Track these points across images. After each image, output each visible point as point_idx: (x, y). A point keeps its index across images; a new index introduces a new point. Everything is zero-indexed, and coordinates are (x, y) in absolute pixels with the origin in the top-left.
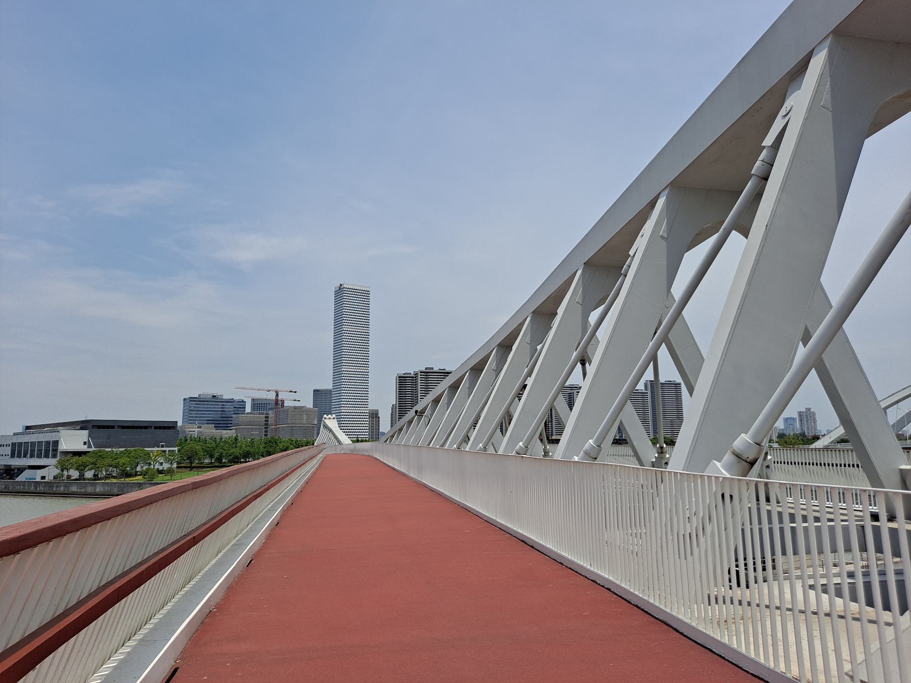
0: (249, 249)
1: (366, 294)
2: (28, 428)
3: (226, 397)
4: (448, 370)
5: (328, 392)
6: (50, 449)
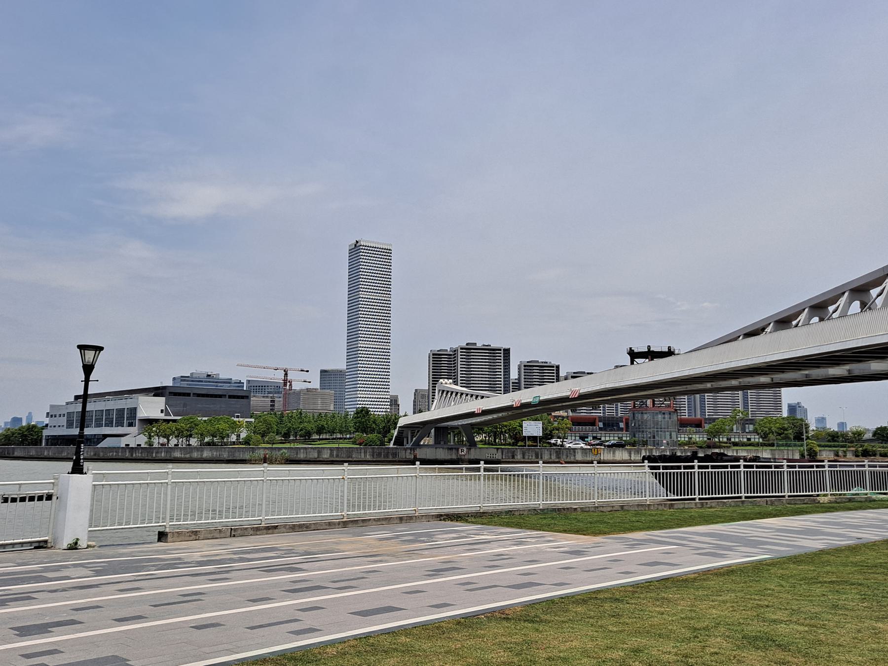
0: (198, 198)
1: (387, 252)
3: (223, 376)
4: (493, 346)
5: (339, 374)
6: (129, 417)
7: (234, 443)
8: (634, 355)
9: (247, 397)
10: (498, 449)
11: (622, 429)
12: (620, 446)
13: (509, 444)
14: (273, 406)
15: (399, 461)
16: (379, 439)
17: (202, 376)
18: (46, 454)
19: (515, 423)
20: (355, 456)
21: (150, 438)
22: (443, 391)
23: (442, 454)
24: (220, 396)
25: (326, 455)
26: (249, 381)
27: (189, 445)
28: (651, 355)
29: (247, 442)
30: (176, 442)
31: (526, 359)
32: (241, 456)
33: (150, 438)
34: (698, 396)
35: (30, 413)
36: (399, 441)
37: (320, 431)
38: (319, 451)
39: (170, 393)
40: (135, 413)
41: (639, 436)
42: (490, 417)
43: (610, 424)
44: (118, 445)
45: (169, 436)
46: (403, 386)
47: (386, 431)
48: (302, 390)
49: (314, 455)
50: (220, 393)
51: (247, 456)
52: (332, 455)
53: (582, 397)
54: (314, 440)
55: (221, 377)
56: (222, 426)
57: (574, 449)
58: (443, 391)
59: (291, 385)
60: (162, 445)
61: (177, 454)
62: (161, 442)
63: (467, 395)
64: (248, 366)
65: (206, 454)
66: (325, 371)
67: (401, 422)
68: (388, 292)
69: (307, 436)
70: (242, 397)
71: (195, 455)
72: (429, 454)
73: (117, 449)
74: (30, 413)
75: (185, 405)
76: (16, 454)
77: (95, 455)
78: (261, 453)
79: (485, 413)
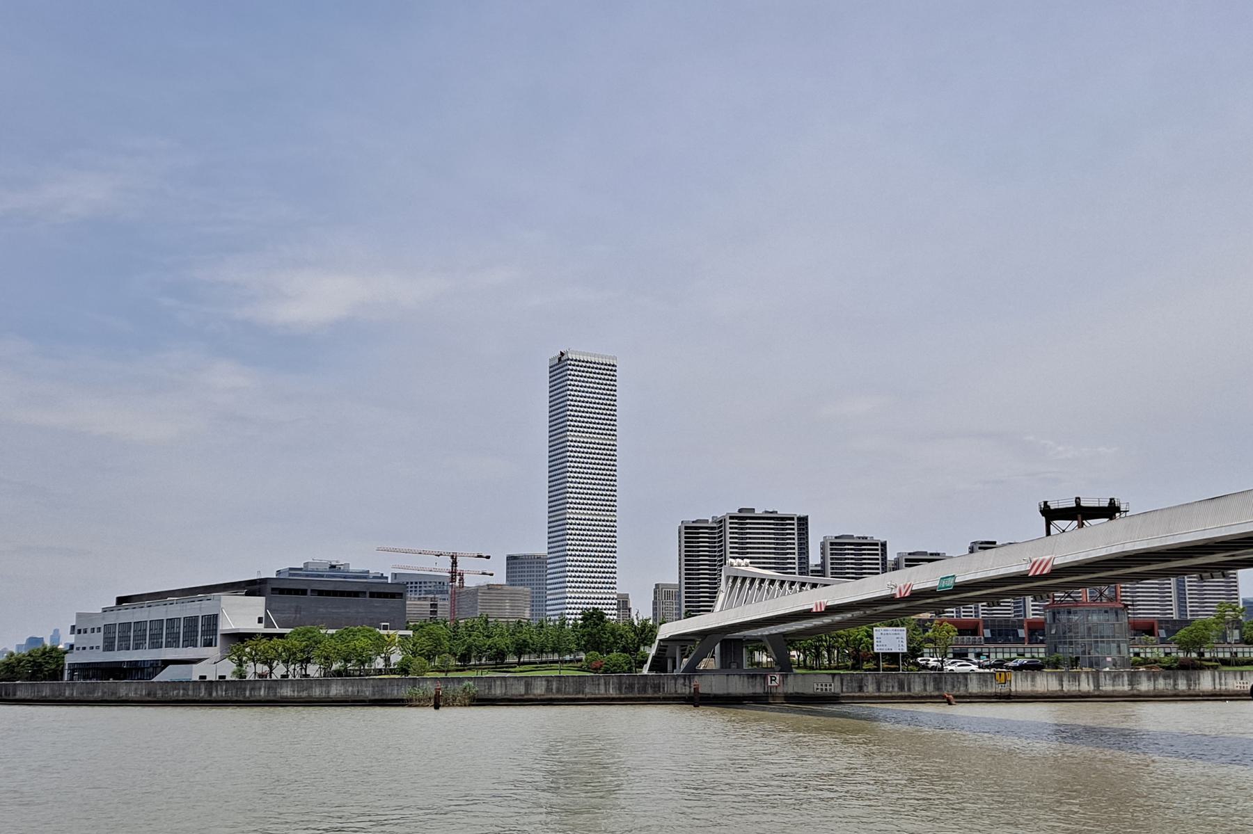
0: (316, 296)
2: (121, 600)
3: (355, 567)
4: (782, 512)
5: (539, 560)
7: (380, 672)
8: (1050, 514)
9: (401, 595)
10: (834, 675)
11: (1021, 641)
12: (1034, 667)
13: (847, 668)
14: (434, 612)
15: (665, 699)
16: (614, 661)
17: (321, 568)
18: (67, 694)
19: (859, 632)
20: (589, 691)
21: (240, 665)
22: (735, 578)
23: (737, 685)
24: (356, 594)
25: (539, 690)
26: (395, 575)
27: (306, 675)
28: (1080, 513)
29: (404, 669)
30: (284, 672)
31: (833, 533)
32: (396, 693)
33: (240, 665)
34: (1173, 580)
35: (56, 631)
36: (659, 664)
37: (519, 651)
38: (528, 682)
39: (273, 589)
40: (216, 625)
41: (1065, 652)
42: (838, 618)
43: (1004, 633)
44: (187, 678)
45: (272, 660)
46: (640, 576)
47: (631, 649)
48: (478, 588)
49: (519, 690)
50: (355, 589)
51: (404, 693)
52: (549, 689)
53: (1058, 572)
54: (511, 665)
55: (352, 568)
56: (361, 643)
57: (965, 674)
58: (735, 578)
59: (462, 579)
60: (261, 676)
61: (287, 692)
62: (259, 671)
63: (772, 582)
64: (395, 551)
65: (336, 690)
67: (665, 631)
69: (498, 659)
70: (393, 595)
71: (317, 692)
72: (709, 685)
73: (185, 684)
74: (56, 631)
75: (298, 610)
76: (20, 694)
77: (149, 695)
78: (430, 688)
79: (831, 610)
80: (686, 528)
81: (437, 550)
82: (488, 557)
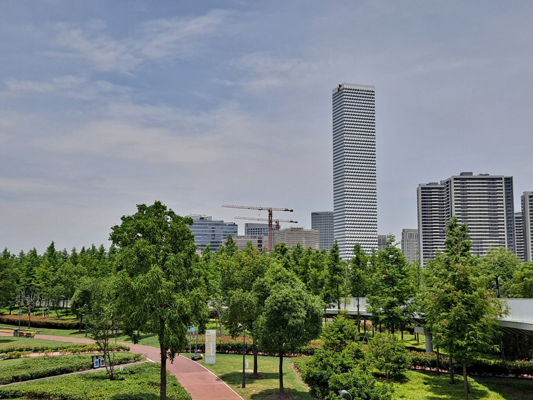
5: (329, 216)
55: (213, 219)
66: (316, 214)
68: (372, 133)
80: (422, 188)
81: (259, 206)
82: (292, 211)
